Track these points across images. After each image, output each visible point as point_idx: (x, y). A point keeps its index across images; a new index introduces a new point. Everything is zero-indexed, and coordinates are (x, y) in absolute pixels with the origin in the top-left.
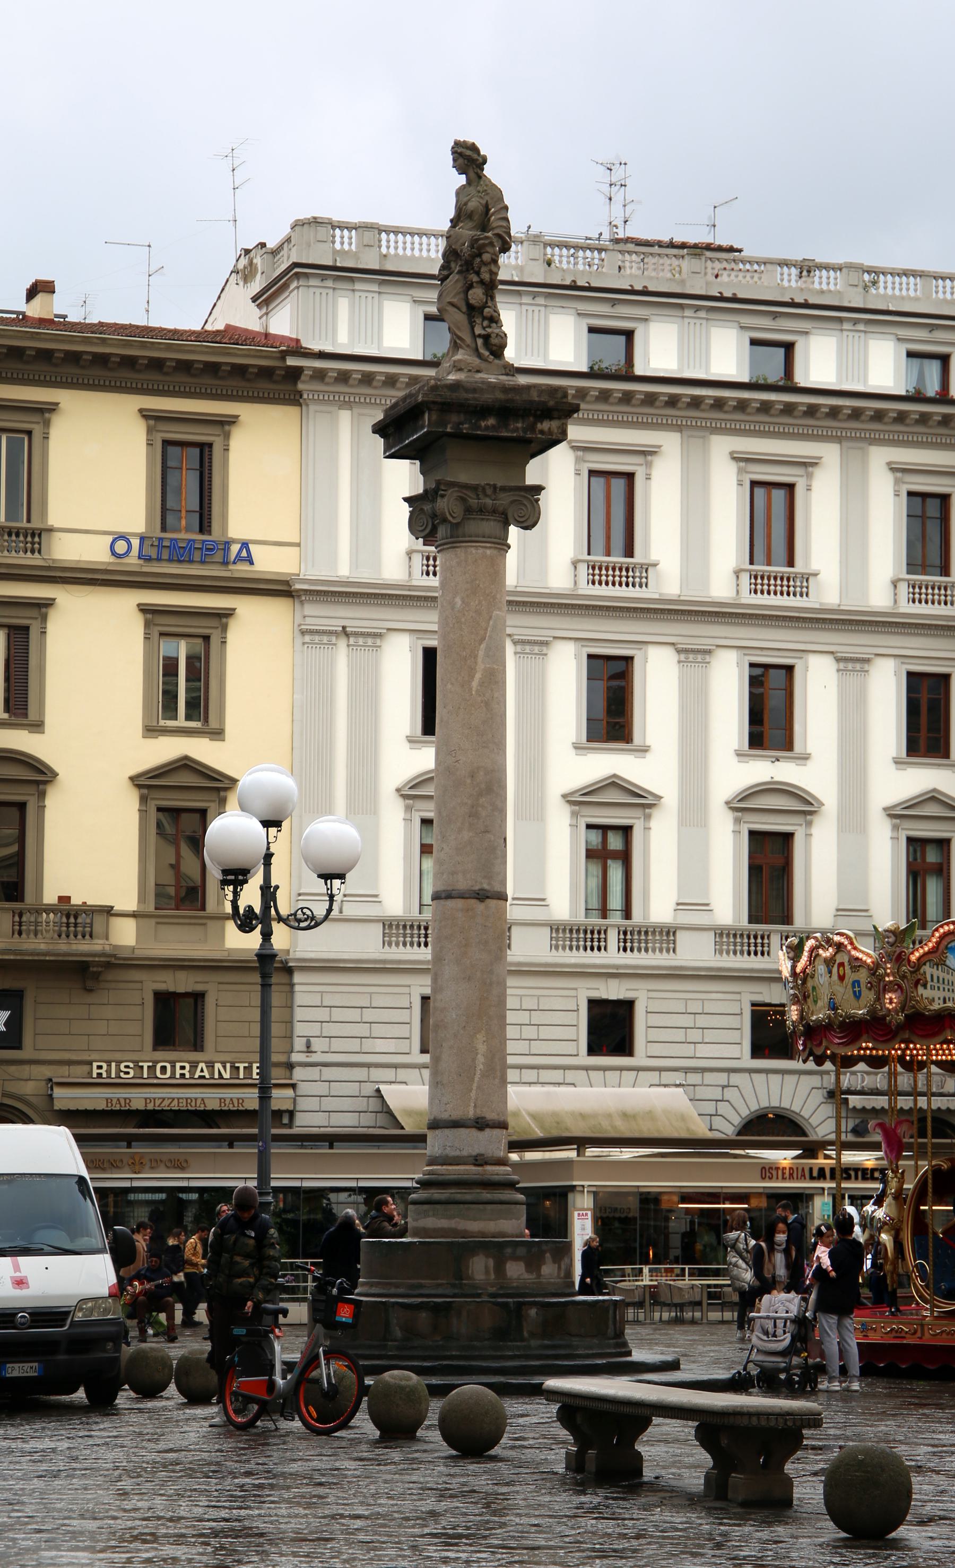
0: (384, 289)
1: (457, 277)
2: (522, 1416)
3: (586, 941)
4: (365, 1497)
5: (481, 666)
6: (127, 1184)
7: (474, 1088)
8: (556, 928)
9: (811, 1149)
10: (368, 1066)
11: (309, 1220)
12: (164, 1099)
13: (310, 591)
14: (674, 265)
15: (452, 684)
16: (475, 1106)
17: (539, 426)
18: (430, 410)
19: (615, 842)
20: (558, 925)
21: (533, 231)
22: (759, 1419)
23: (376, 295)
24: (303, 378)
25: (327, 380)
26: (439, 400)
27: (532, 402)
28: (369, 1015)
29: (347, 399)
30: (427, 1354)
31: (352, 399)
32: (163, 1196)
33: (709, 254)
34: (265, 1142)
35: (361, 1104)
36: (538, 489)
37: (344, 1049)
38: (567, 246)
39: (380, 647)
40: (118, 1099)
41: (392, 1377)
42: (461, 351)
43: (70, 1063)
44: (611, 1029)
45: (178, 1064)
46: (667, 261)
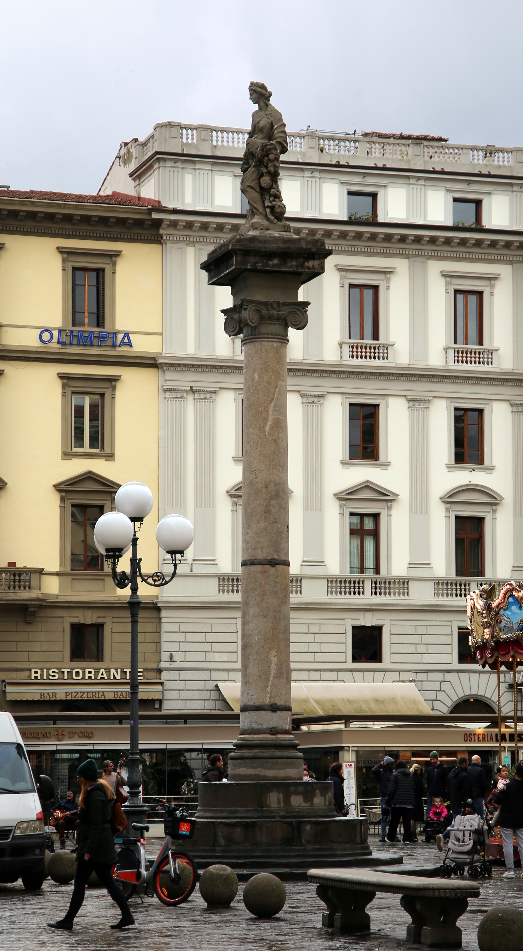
0: (215, 168)
1: (253, 169)
2: (300, 893)
3: (350, 589)
4: (194, 943)
5: (271, 417)
6: (53, 748)
7: (270, 685)
8: (331, 580)
9: (495, 723)
10: (210, 670)
11: (172, 770)
12: (78, 693)
13: (169, 364)
14: (403, 151)
15: (253, 429)
16: (270, 697)
17: (306, 264)
18: (236, 254)
19: (369, 524)
20: (332, 578)
21: (312, 129)
22: (439, 892)
23: (210, 172)
24: (163, 226)
25: (178, 227)
26: (242, 248)
27: (302, 249)
28: (210, 637)
29: (191, 239)
30: (240, 855)
31: (195, 240)
32: (77, 756)
33: (426, 143)
34: (134, 721)
35: (206, 695)
36: (306, 304)
37: (194, 659)
38: (334, 139)
39: (215, 399)
40: (48, 693)
41: (214, 869)
42: (256, 217)
43: (17, 670)
44: (367, 645)
45: (87, 670)
46: (398, 148)
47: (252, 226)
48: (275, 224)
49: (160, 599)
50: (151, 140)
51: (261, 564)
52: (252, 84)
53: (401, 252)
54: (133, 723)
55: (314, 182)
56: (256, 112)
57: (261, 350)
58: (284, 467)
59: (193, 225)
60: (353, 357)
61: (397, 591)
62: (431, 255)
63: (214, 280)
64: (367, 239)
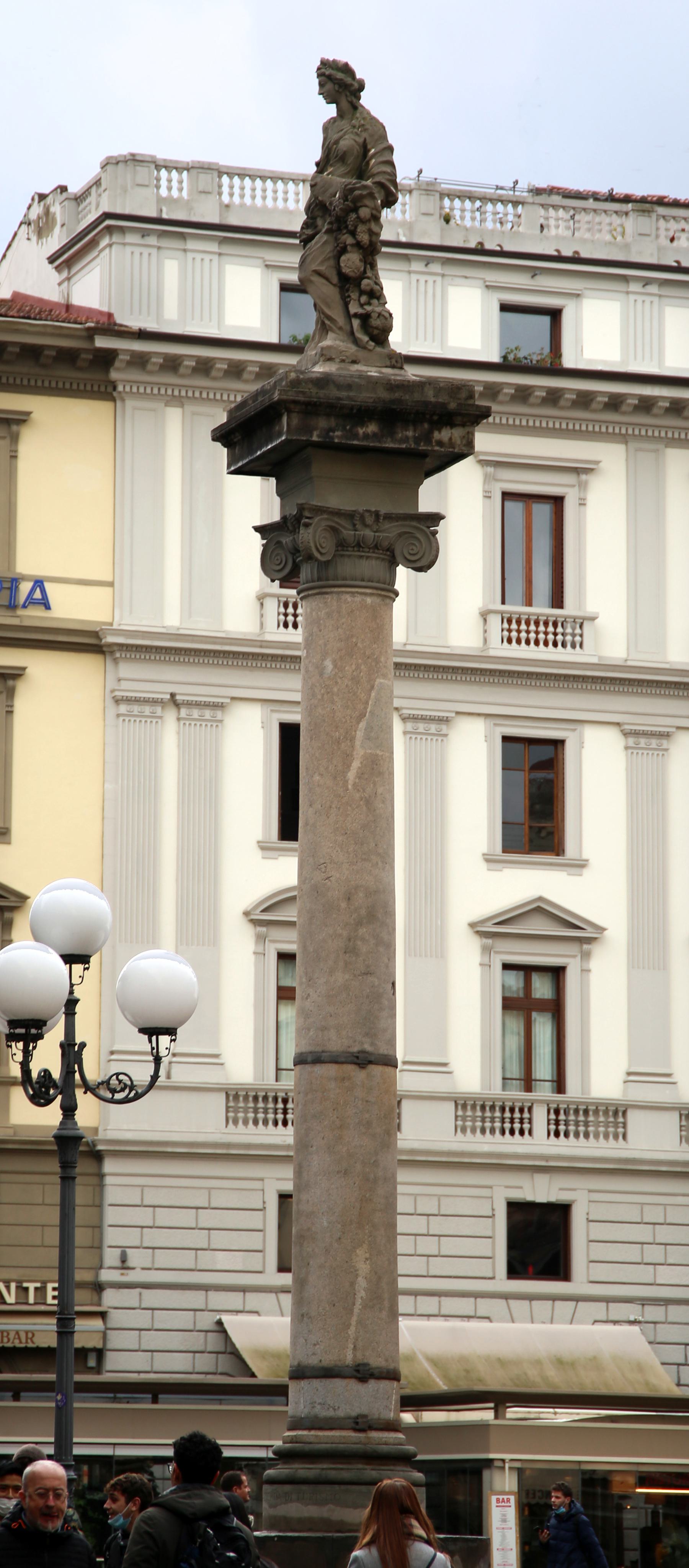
0: (227, 249)
1: (325, 238)
5: (359, 752)
10: (206, 1288)
16: (355, 1349)
17: (436, 435)
18: (289, 412)
19: (542, 988)
20: (466, 1100)
21: (426, 176)
23: (215, 258)
24: (117, 364)
26: (301, 398)
27: (427, 403)
28: (207, 1218)
29: (176, 393)
31: (183, 393)
33: (661, 210)
34: (65, 1396)
35: (196, 1341)
36: (436, 518)
37: (172, 1264)
38: (472, 197)
39: (221, 721)
42: (331, 335)
44: (539, 1243)
47: (322, 355)
48: (370, 350)
49: (101, 1136)
50: (94, 188)
51: (336, 1062)
52: (324, 63)
53: (610, 430)
54: (62, 1400)
55: (430, 283)
56: (332, 121)
57: (339, 612)
58: (384, 857)
59: (180, 365)
60: (510, 641)
61: (602, 1129)
62: (673, 438)
63: (240, 464)
64: (539, 401)
